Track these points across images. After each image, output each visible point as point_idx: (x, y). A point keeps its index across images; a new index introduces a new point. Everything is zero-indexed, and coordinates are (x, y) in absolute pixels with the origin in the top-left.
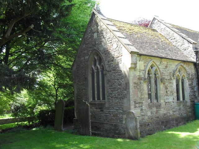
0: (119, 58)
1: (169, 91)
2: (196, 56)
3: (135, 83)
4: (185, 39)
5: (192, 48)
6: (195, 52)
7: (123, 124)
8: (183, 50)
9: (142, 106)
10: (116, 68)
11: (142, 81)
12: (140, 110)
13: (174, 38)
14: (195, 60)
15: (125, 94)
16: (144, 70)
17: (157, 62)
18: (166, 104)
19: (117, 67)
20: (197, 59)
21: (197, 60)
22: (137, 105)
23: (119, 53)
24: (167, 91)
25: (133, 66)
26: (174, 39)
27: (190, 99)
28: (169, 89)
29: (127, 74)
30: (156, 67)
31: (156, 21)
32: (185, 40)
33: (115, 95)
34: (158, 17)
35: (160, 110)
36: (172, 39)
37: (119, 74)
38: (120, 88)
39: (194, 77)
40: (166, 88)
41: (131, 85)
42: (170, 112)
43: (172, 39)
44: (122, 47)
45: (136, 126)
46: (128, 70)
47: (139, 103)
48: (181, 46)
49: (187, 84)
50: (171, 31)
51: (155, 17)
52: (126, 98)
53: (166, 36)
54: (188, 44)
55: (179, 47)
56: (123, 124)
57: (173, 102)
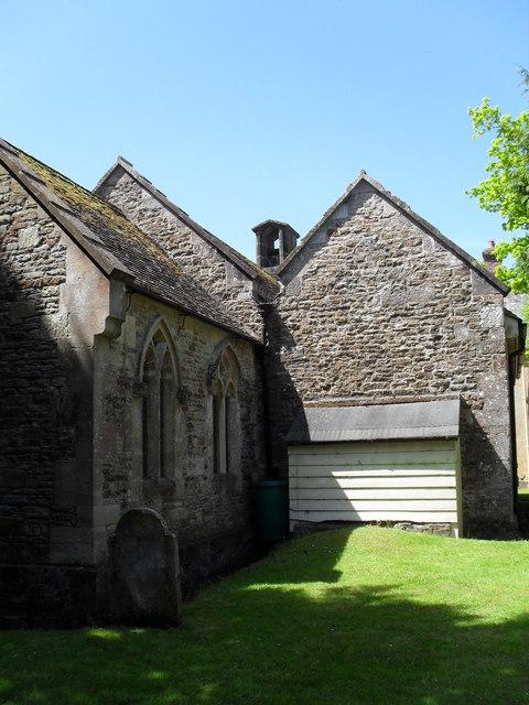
0: (45, 292)
1: (195, 437)
2: (265, 321)
3: (108, 398)
4: (228, 259)
5: (249, 295)
6: (260, 307)
7: (49, 564)
8: (218, 298)
9: (125, 491)
10: (27, 331)
11: (129, 394)
12: (117, 507)
13: (187, 248)
14: (257, 335)
15: (64, 441)
16: (136, 351)
17: (172, 321)
18: (186, 485)
19: (34, 324)
20: (265, 330)
21: (265, 338)
22: (112, 485)
23: (50, 269)
24: (190, 437)
25: (112, 328)
26: (190, 253)
27: (243, 471)
28: (197, 431)
29: (82, 358)
30: (168, 343)
31: (124, 179)
32: (227, 263)
33: (13, 444)
34: (131, 165)
35: (173, 507)
36: (178, 254)
37: (44, 354)
38: (41, 416)
39: (255, 393)
40: (190, 426)
41: (98, 402)
42: (197, 515)
43: (178, 254)
44: (63, 249)
45: (168, 571)
46: (91, 340)
47: (119, 477)
48: (213, 281)
49: (238, 415)
50: (181, 224)
51: (123, 164)
52: (73, 455)
53: (156, 239)
54: (240, 278)
55: (203, 285)
56: (49, 564)
57: (205, 479)
